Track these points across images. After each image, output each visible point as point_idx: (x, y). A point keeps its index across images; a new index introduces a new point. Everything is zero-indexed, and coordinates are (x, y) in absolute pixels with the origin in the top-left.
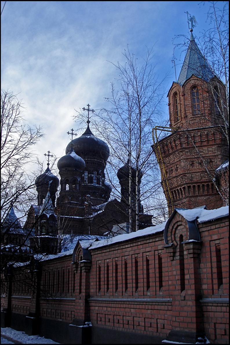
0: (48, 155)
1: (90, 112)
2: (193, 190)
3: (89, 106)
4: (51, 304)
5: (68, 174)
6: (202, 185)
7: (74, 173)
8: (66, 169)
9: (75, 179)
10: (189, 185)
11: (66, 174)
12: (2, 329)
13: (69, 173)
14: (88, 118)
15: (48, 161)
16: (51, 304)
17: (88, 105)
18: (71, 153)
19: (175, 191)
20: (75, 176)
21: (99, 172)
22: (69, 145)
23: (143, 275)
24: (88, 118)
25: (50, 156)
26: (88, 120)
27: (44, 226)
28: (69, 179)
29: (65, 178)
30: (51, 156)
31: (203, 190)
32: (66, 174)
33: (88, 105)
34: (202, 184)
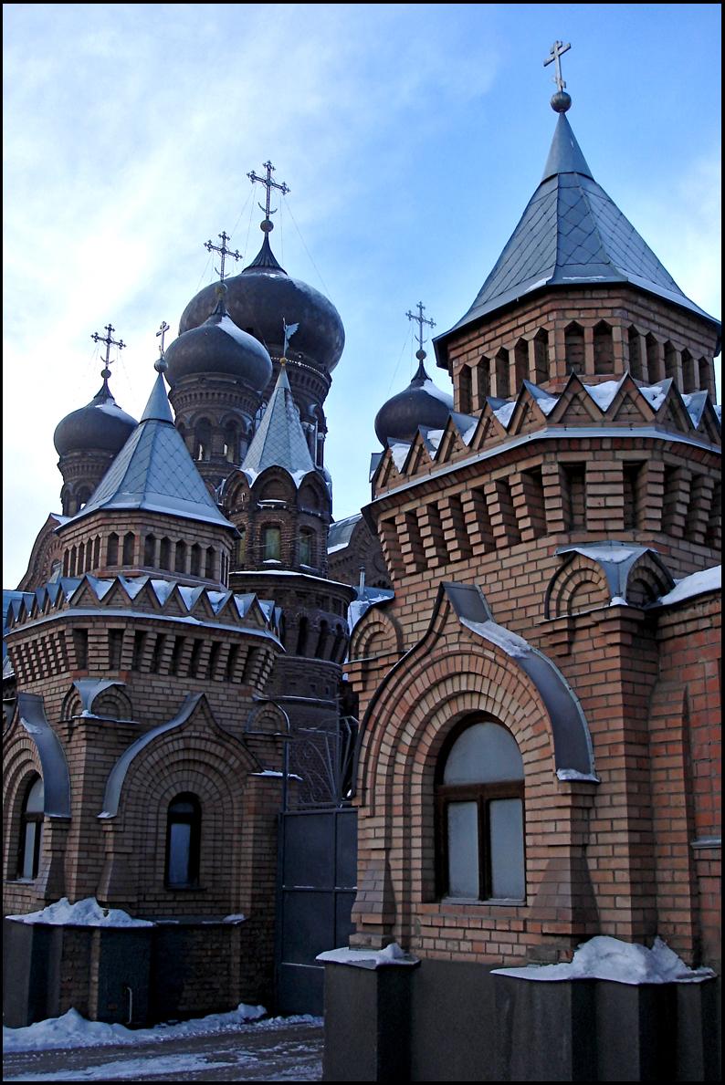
0: (226, 255)
1: (275, 192)
2: (106, 647)
3: (269, 170)
4: (387, 850)
5: (90, 468)
6: (555, 468)
7: (231, 396)
8: (202, 379)
9: (235, 419)
10: (115, 626)
11: (198, 396)
12: (5, 1030)
13: (219, 394)
14: (268, 212)
15: (107, 362)
16: (387, 850)
17: (269, 167)
18: (220, 320)
19: (412, 516)
20: (237, 410)
21: (307, 408)
22: (199, 302)
23: (642, 684)
24: (268, 212)
25: (115, 343)
26: (267, 217)
27: (278, 526)
28: (208, 416)
29: (198, 413)
30: (116, 346)
31: (542, 487)
32: (198, 396)
33: (269, 167)
34: (561, 464)
